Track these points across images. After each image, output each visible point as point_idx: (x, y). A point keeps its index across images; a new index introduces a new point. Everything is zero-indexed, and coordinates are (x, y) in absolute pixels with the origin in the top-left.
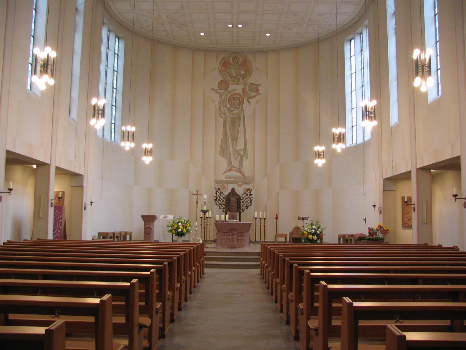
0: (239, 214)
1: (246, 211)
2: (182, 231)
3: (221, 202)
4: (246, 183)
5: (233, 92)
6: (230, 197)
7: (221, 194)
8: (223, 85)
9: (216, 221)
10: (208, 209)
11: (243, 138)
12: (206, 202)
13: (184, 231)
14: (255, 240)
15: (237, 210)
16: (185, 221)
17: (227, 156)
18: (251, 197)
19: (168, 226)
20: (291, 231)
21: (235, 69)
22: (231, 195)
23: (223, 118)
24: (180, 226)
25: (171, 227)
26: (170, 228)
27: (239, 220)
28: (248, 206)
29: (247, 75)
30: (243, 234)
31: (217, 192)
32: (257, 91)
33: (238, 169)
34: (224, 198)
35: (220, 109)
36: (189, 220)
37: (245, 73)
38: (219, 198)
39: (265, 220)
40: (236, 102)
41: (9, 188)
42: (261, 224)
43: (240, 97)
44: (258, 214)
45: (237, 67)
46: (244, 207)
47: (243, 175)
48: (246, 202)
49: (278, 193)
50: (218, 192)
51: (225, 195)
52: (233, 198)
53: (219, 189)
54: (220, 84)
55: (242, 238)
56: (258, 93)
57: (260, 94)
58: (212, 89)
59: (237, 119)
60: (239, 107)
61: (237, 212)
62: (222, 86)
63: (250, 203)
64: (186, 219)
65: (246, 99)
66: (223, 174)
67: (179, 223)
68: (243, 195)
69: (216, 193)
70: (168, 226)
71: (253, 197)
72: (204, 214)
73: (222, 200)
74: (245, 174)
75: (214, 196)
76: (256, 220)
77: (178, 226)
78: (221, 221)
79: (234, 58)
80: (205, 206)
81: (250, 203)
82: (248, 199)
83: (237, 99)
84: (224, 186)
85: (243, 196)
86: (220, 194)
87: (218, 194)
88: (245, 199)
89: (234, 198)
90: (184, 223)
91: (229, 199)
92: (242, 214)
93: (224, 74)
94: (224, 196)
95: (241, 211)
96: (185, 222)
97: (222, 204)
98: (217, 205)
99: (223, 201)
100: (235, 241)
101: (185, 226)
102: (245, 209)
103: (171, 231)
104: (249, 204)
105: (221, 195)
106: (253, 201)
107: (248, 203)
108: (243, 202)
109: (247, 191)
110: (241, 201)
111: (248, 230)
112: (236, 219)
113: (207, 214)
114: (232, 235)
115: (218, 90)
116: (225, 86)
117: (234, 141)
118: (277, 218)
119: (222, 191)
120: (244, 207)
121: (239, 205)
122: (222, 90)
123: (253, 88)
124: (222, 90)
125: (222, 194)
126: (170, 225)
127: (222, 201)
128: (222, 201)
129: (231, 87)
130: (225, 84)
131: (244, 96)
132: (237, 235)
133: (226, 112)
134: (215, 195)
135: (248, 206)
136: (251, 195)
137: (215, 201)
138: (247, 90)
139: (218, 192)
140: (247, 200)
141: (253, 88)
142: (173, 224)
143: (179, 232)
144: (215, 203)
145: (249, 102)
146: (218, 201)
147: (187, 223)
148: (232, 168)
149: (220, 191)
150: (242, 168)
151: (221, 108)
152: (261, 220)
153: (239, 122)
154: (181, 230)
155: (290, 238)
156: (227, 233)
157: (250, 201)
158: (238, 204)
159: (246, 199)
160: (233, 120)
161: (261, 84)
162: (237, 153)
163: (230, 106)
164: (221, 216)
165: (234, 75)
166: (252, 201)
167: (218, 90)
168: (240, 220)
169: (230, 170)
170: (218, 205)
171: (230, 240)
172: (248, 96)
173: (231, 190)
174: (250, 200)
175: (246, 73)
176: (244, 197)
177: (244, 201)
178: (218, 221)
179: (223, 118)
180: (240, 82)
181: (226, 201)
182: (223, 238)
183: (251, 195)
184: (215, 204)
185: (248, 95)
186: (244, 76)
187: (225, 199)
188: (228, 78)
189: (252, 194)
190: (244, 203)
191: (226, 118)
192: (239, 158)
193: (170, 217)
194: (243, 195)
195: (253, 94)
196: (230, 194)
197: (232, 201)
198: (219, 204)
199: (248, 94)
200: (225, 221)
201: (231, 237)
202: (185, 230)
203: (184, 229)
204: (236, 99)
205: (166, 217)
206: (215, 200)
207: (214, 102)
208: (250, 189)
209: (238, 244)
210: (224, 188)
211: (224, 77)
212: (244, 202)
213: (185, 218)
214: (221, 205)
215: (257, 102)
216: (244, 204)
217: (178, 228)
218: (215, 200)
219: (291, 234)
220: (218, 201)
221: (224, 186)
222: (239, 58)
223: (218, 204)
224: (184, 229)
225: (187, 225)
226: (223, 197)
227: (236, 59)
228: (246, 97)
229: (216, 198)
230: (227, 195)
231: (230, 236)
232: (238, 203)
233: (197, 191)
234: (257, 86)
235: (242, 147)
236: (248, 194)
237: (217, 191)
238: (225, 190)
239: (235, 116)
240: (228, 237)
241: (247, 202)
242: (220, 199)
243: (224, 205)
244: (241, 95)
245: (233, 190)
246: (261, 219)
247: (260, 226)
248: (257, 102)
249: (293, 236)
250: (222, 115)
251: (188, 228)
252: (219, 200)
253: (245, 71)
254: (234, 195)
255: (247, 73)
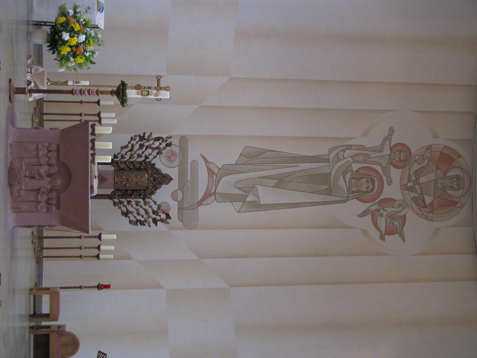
0: (108, 195)
1: (117, 211)
2: (64, 43)
3: (137, 151)
4: (181, 209)
5: (384, 178)
6: (150, 171)
7: (158, 151)
8: (400, 154)
9: (93, 127)
10: (129, 102)
11: (286, 202)
12: (149, 97)
13: (63, 47)
14: (45, 235)
15: (119, 190)
16: (90, 51)
17: (242, 164)
18: (150, 222)
19: (75, 9)
20: (68, 329)
21: (436, 180)
22: (155, 175)
23: (329, 154)
24: (77, 37)
25: (75, 16)
26: (71, 12)
27: (97, 195)
28: (129, 215)
29: (422, 209)
30: (54, 208)
31: (161, 141)
32: (389, 232)
33: (213, 190)
34: (147, 157)
35: (347, 149)
36: (92, 63)
37: (427, 204)
38: (146, 144)
39: (94, 257)
40: (364, 185)
41: (101, 112)
42: (85, 248)
43: (373, 193)
44: (109, 242)
45: (439, 185)
46: (125, 206)
47: (200, 203)
48: (137, 210)
49: (159, 287)
50: (160, 144)
51: (155, 159)
52: (148, 179)
53: (167, 145)
54: (403, 148)
55: (43, 204)
56: (384, 233)
57: (382, 238)
58: (391, 131)
59: (327, 187)
60: (353, 192)
61: (113, 190)
62: (397, 153)
63: (135, 220)
64: (95, 56)
65: (370, 207)
66: (201, 154)
67: (84, 36)
68: (155, 203)
69: (158, 137)
70: (75, 9)
71: (149, 226)
72: (115, 89)
73: (143, 153)
74: (201, 208)
75: (151, 134)
76: (95, 237)
77: (78, 33)
78: (93, 141)
79: (458, 177)
80: (138, 94)
81: (135, 220)
82: (145, 216)
83: (371, 187)
84: (173, 158)
85: (152, 203)
86: (157, 148)
87: (157, 144)
88: (144, 207)
89: (147, 181)
90: (85, 51)
91: (146, 169)
92: (109, 202)
93: (423, 155)
94: (151, 157)
95: (115, 200)
96: (87, 54)
97: (133, 152)
98: (130, 140)
99: (139, 156)
100: (35, 184)
101: (78, 53)
102: (120, 208)
103: (63, 13)
104: (132, 218)
105: (153, 149)
106: (139, 227)
107: (135, 215)
108: (137, 203)
109: (164, 213)
110: (141, 198)
111: (66, 222)
112: (98, 188)
113: (113, 101)
114: (49, 175)
115: (390, 144)
116: (397, 160)
117: (277, 181)
118: (100, 287)
119: (164, 152)
120: (125, 206)
121: (131, 195)
122: (389, 152)
123: (395, 222)
124: (391, 152)
125: (158, 153)
126: (80, 12)
127: (140, 152)
128: (140, 152)
129: (395, 173)
130: (402, 159)
131: (376, 201)
132: (51, 190)
133: (340, 163)
134: (154, 136)
135: (129, 215)
136: (155, 221)
137: (140, 136)
138: (390, 210)
139: (160, 144)
140: (142, 212)
141: (395, 222)
142: (82, 20)
143: (62, 35)
144: (136, 136)
145: (363, 215)
146: (139, 143)
147: (87, 59)
148: (215, 177)
149: (164, 149)
150: (216, 199)
151: (351, 149)
152: (95, 248)
153: (320, 193)
154: (66, 39)
155: (48, 327)
156: (58, 158)
157: (140, 221)
158: (133, 191)
159: (146, 212)
160: (324, 179)
161: (403, 239)
162: (251, 188)
163: (354, 171)
164: (110, 142)
165: (422, 180)
166: (141, 224)
167: (390, 144)
168: (98, 196)
169: (211, 172)
170: (129, 143)
171: (36, 168)
172: (378, 210)
173: (166, 174)
174: (143, 219)
175: (426, 207)
176: (151, 207)
177: (141, 206)
178: (94, 130)
179: (329, 154)
180: (407, 192)
181: (141, 163)
182: (40, 145)
183: (155, 221)
184: (133, 135)
185: (380, 210)
186: (420, 202)
187: (144, 160)
188: (416, 167)
189: (156, 225)
190: (135, 206)
191: (328, 161)
192: (240, 192)
193: (99, 19)
194: (155, 203)
195: (382, 223)
196: (158, 171)
197: (141, 177)
198: (133, 146)
199: (382, 211)
200: (92, 152)
201: (43, 170)
202: (66, 50)
203: (69, 49)
204: (370, 184)
205: (100, 9)
206: (142, 135)
207: (365, 135)
208: (168, 220)
209: (22, 192)
210: (169, 158)
211: (417, 158)
212: (137, 205)
213: (97, 53)
214: (129, 151)
215: (364, 232)
216: (132, 207)
217: (73, 32)
218: (142, 135)
219: (60, 330)
220: (139, 143)
221: (173, 158)
222: (458, 190)
223: (132, 142)
224: (69, 49)
225: (81, 58)
226: (149, 155)
227: (455, 183)
228: (374, 208)
229: (146, 137)
230: (154, 164)
231: (47, 167)
232: (136, 190)
233: (168, 87)
234: (400, 232)
235: (264, 200)
236: (157, 215)
237: (163, 141)
238: (164, 159)
239: (332, 181)
240: (43, 160)
241: (138, 214)
242: (144, 148)
243: (130, 158)
244: (379, 196)
245: (167, 179)
246: (99, 248)
247: (80, 248)
248: (364, 232)
249: (53, 337)
250: (337, 151)
251: (72, 59)
252: (141, 146)
253: (431, 204)
254: (154, 181)
255: (426, 209)
